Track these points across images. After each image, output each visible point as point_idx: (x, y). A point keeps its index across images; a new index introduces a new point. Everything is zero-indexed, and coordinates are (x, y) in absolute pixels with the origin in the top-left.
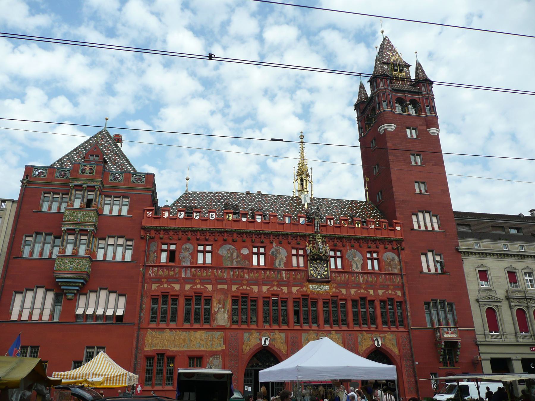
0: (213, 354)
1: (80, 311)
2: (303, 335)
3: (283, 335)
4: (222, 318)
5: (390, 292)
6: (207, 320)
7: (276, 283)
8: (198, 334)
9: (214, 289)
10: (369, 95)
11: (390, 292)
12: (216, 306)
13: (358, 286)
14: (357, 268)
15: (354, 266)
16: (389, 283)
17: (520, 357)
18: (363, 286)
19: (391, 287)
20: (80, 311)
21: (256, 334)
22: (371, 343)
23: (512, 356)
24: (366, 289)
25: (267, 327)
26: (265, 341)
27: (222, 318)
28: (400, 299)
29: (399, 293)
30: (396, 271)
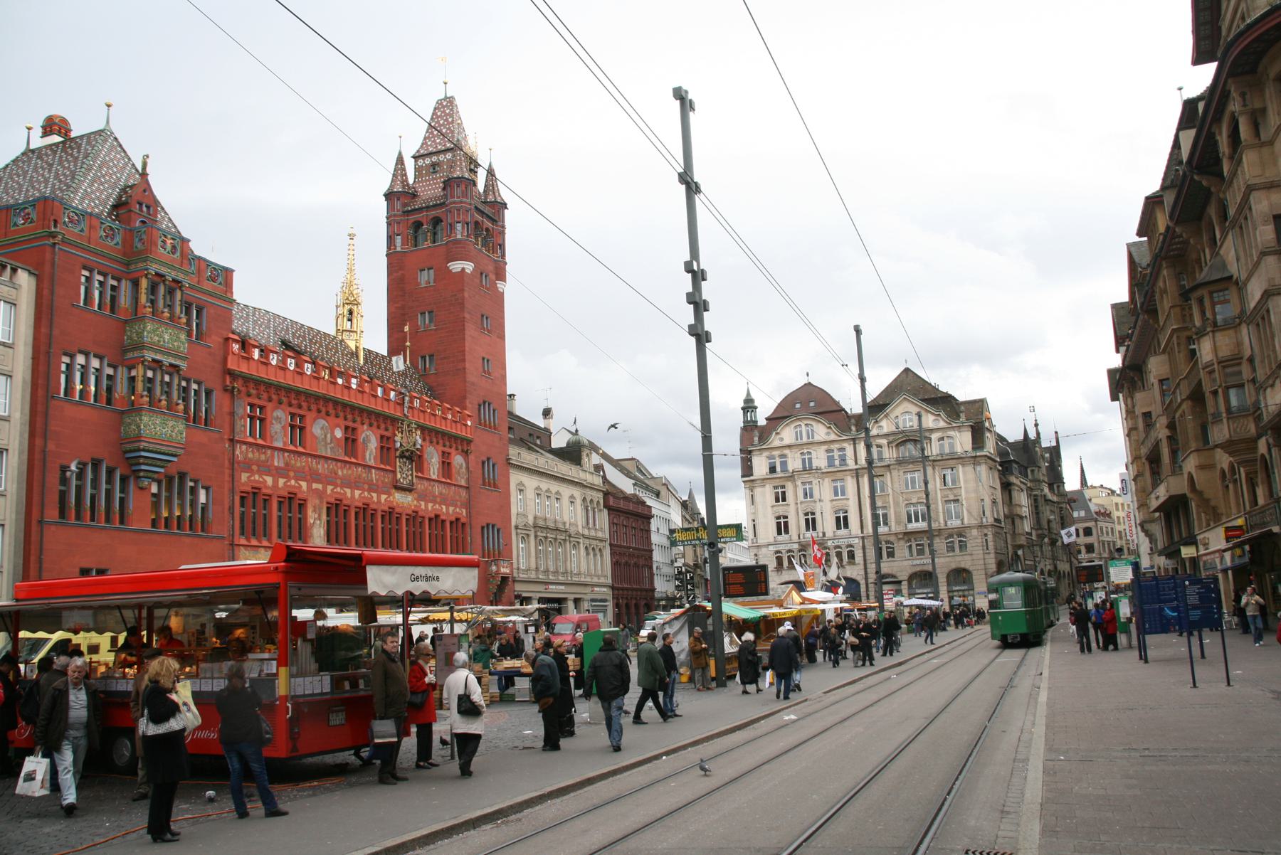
9: (309, 487)
10: (411, 181)
12: (311, 516)
20: (432, 272)
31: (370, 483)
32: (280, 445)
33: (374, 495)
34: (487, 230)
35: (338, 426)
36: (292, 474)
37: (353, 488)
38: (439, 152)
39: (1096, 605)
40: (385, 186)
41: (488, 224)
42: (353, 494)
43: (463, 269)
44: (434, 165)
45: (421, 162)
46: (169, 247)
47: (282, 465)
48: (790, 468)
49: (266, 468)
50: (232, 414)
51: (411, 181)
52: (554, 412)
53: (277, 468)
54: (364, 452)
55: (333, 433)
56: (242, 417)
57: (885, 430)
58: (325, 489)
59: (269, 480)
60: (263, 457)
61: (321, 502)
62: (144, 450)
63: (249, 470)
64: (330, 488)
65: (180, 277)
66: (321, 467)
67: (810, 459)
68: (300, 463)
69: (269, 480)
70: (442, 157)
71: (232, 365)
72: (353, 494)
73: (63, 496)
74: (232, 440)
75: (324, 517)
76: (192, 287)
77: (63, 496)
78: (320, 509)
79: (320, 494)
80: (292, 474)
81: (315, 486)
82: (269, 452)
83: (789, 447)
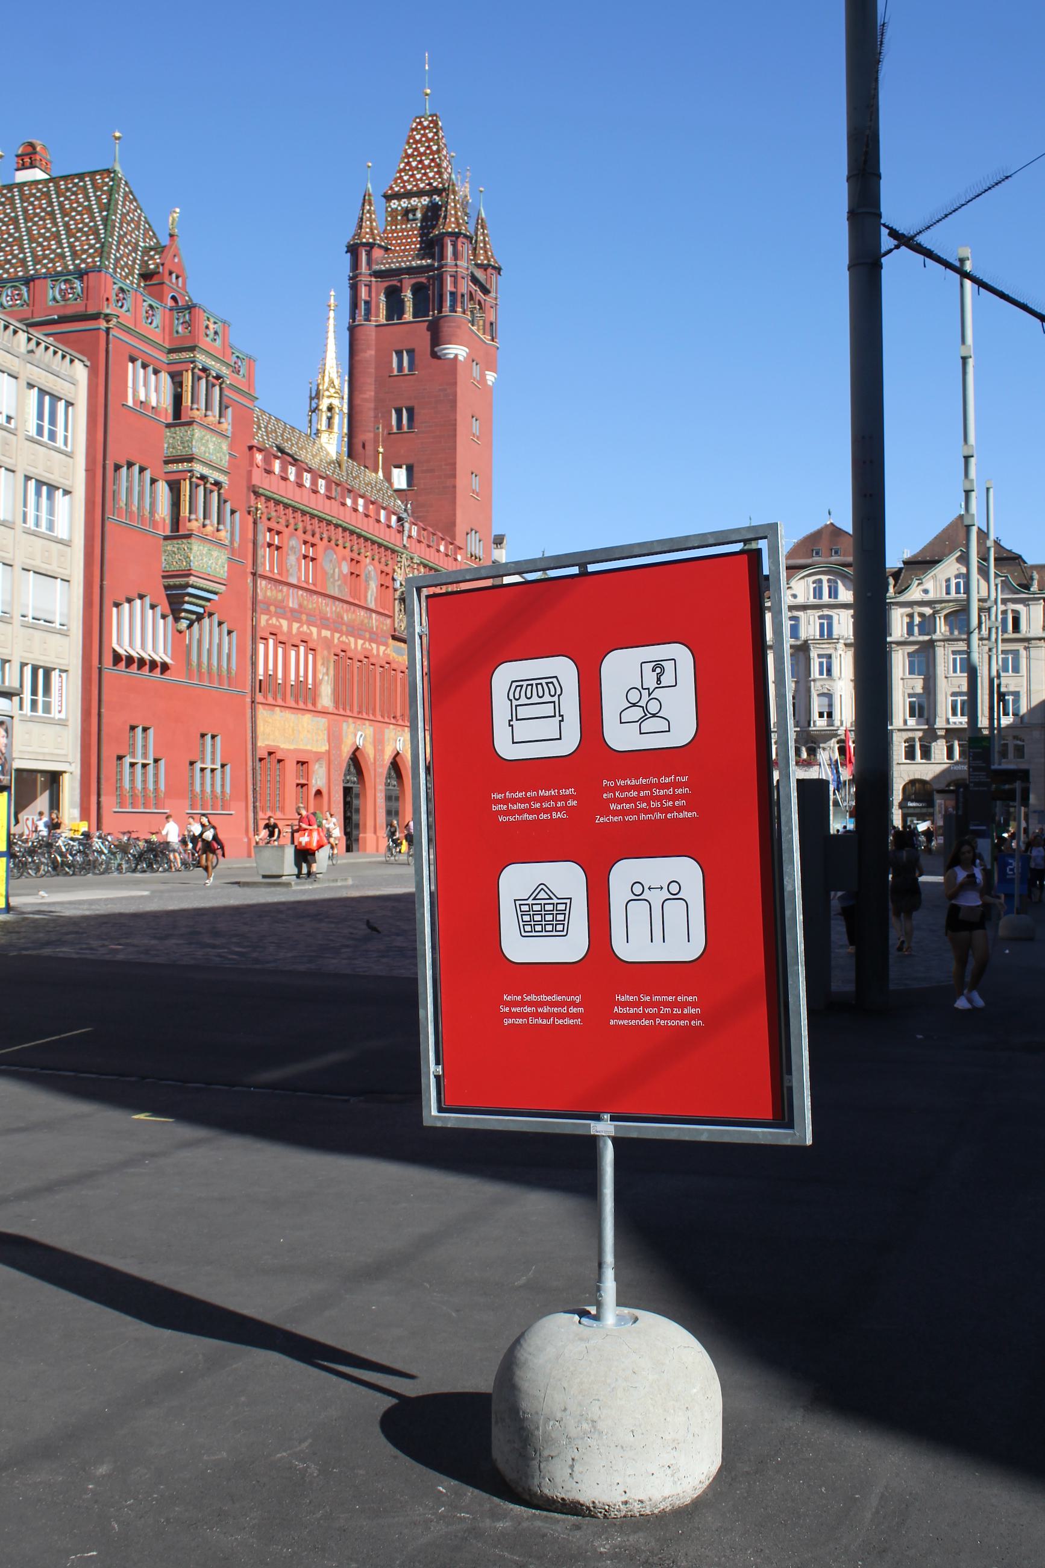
31: (324, 618)
32: (294, 581)
33: (374, 646)
35: (344, 559)
36: (304, 617)
37: (357, 637)
38: (409, 195)
42: (290, 627)
44: (406, 212)
45: (394, 204)
46: (211, 332)
47: (296, 606)
48: (803, 635)
50: (255, 543)
53: (292, 610)
54: (366, 592)
55: (340, 567)
56: (262, 546)
57: (931, 596)
58: (332, 636)
60: (280, 596)
61: (329, 653)
62: (193, 586)
63: (267, 612)
65: (224, 371)
67: (830, 626)
70: (414, 201)
71: (258, 478)
72: (290, 627)
74: (254, 574)
75: (332, 672)
76: (232, 386)
78: (328, 661)
80: (304, 617)
82: (285, 589)
83: (804, 608)
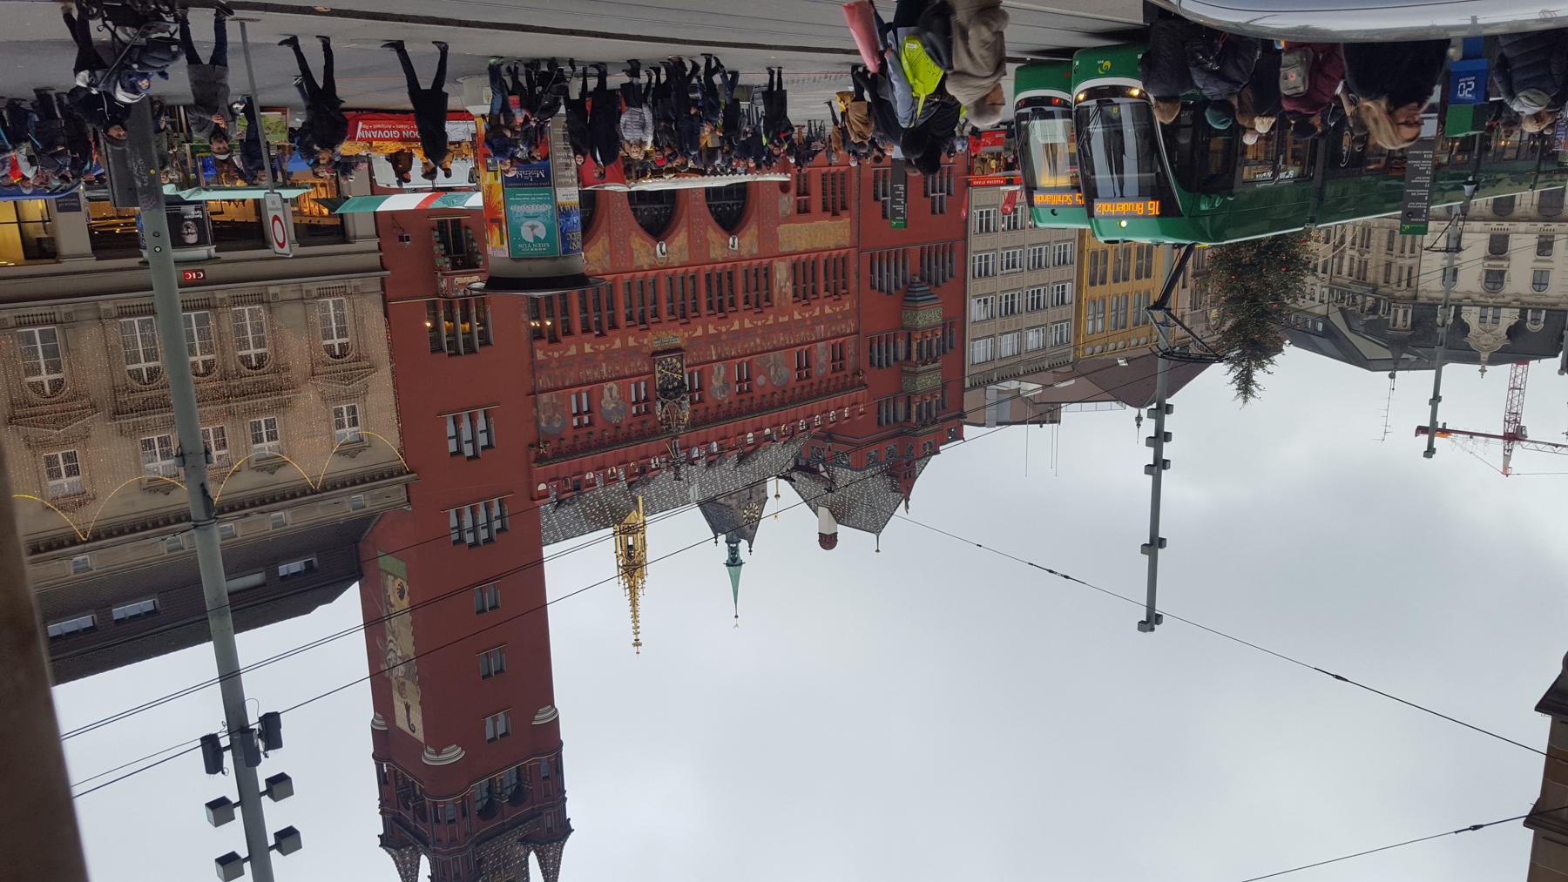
0: (788, 219)
1: (490, 735)
2: (755, 251)
3: (712, 255)
4: (781, 272)
5: (556, 355)
6: (794, 266)
7: (724, 337)
8: (832, 244)
9: (791, 316)
10: (533, 859)
11: (556, 355)
12: (788, 289)
13: (609, 356)
14: (610, 390)
15: (615, 393)
16: (558, 372)
17: (66, 265)
18: (601, 357)
19: (554, 364)
20: (490, 735)
21: (744, 252)
22: (589, 255)
23: (92, 263)
24: (597, 352)
25: (813, 256)
26: (661, 248)
27: (781, 272)
28: (537, 344)
29: (540, 355)
30: (544, 398)
34: (408, 808)
39: (545, 181)
40: (570, 847)
41: (408, 815)
43: (438, 753)
49: (830, 320)
51: (533, 859)
52: (203, 814)
59: (828, 310)
64: (770, 322)
66: (783, 339)
68: (802, 335)
69: (828, 310)
73: (871, 358)
75: (776, 291)
77: (871, 358)
79: (782, 312)
81: (786, 319)
